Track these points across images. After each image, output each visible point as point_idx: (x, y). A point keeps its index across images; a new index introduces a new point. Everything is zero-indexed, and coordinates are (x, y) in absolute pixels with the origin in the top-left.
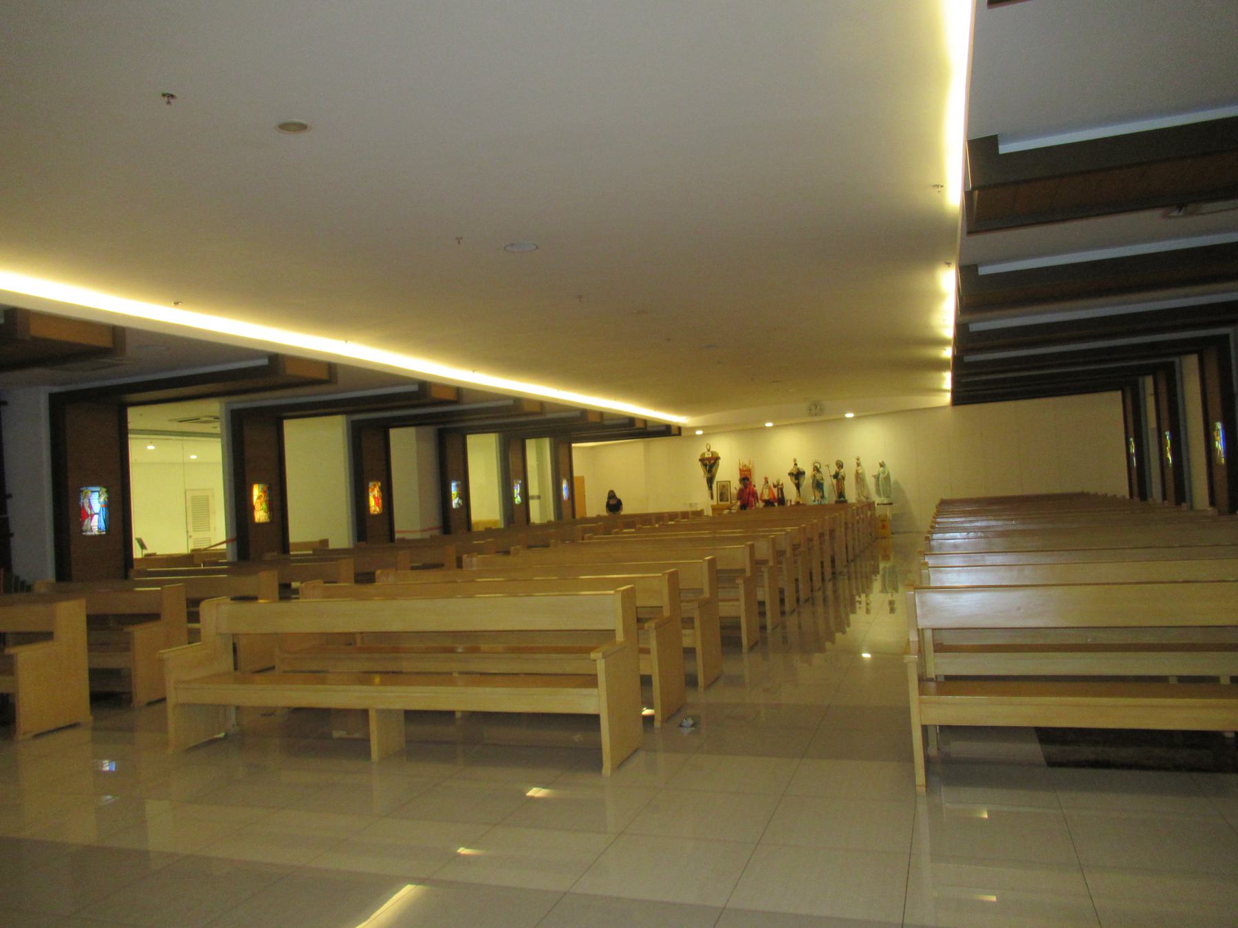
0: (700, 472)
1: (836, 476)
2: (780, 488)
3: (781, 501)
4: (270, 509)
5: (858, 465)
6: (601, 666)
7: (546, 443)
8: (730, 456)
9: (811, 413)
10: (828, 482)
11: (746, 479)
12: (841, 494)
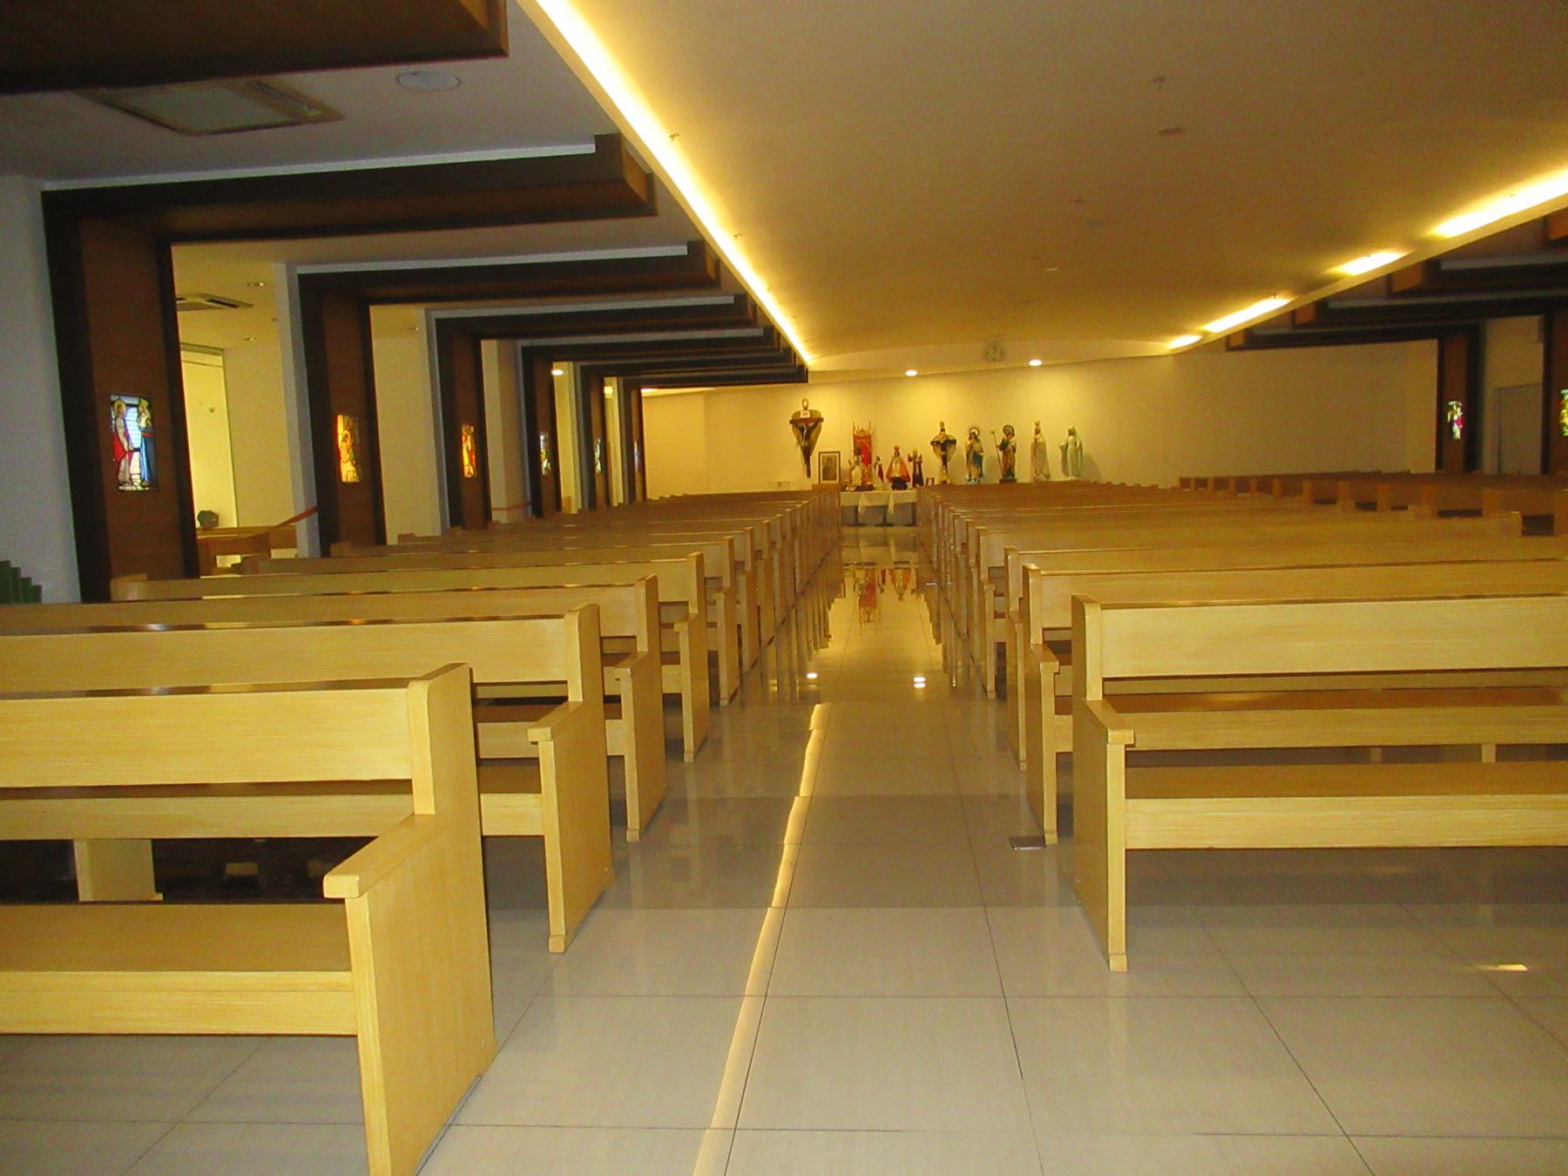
0: (790, 437)
1: (1003, 446)
2: (916, 461)
3: (918, 479)
4: (358, 462)
5: (1038, 432)
6: (547, 754)
7: (1530, 325)
8: (838, 415)
9: (986, 356)
10: (991, 452)
11: (863, 447)
12: (1009, 471)
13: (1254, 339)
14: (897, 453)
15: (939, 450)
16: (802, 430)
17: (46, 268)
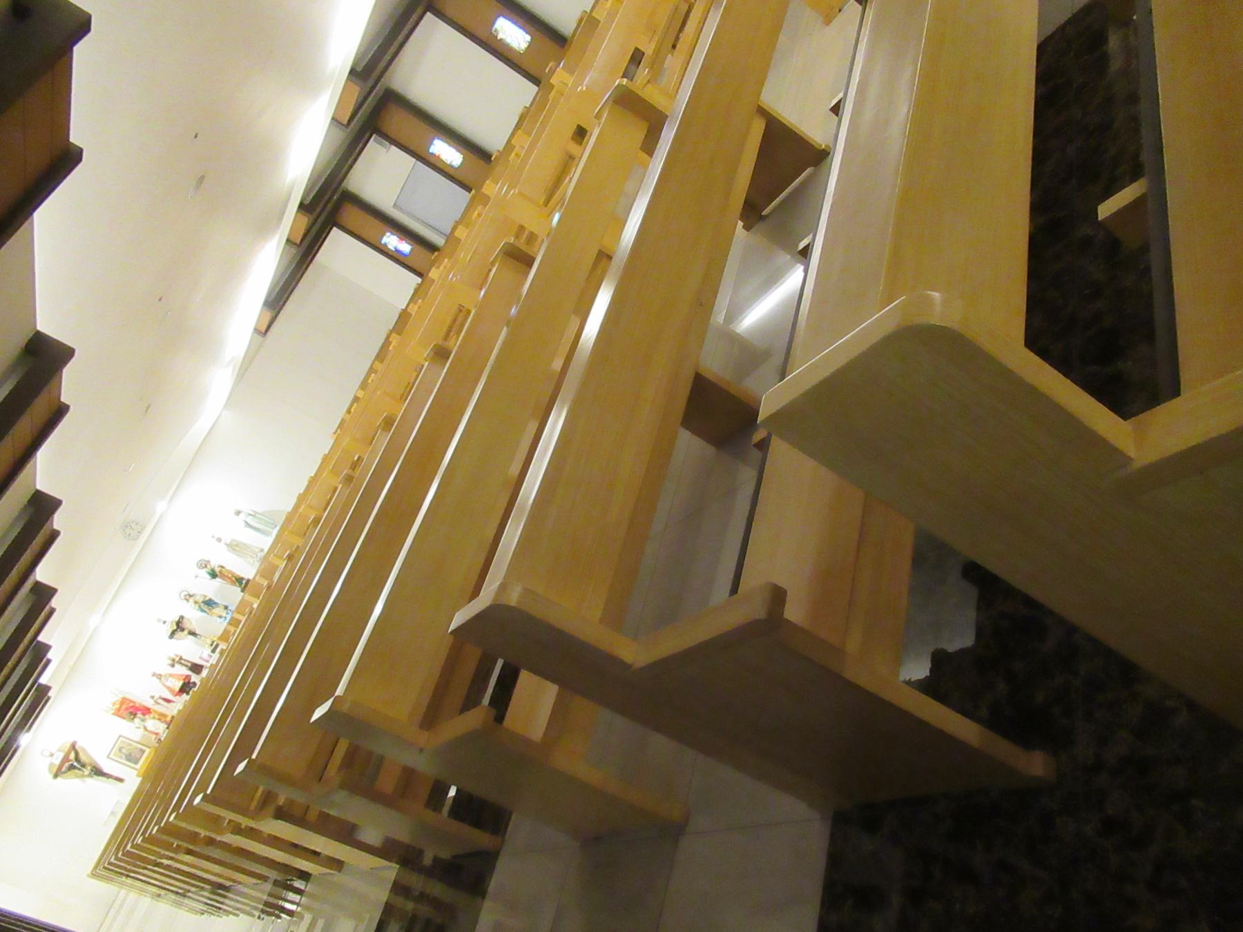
0: (73, 784)
2: (177, 661)
3: (196, 668)
5: (219, 540)
10: (212, 588)
13: (278, 300)
14: (159, 676)
15: (66, 759)
16: (72, 767)
17: (322, 147)
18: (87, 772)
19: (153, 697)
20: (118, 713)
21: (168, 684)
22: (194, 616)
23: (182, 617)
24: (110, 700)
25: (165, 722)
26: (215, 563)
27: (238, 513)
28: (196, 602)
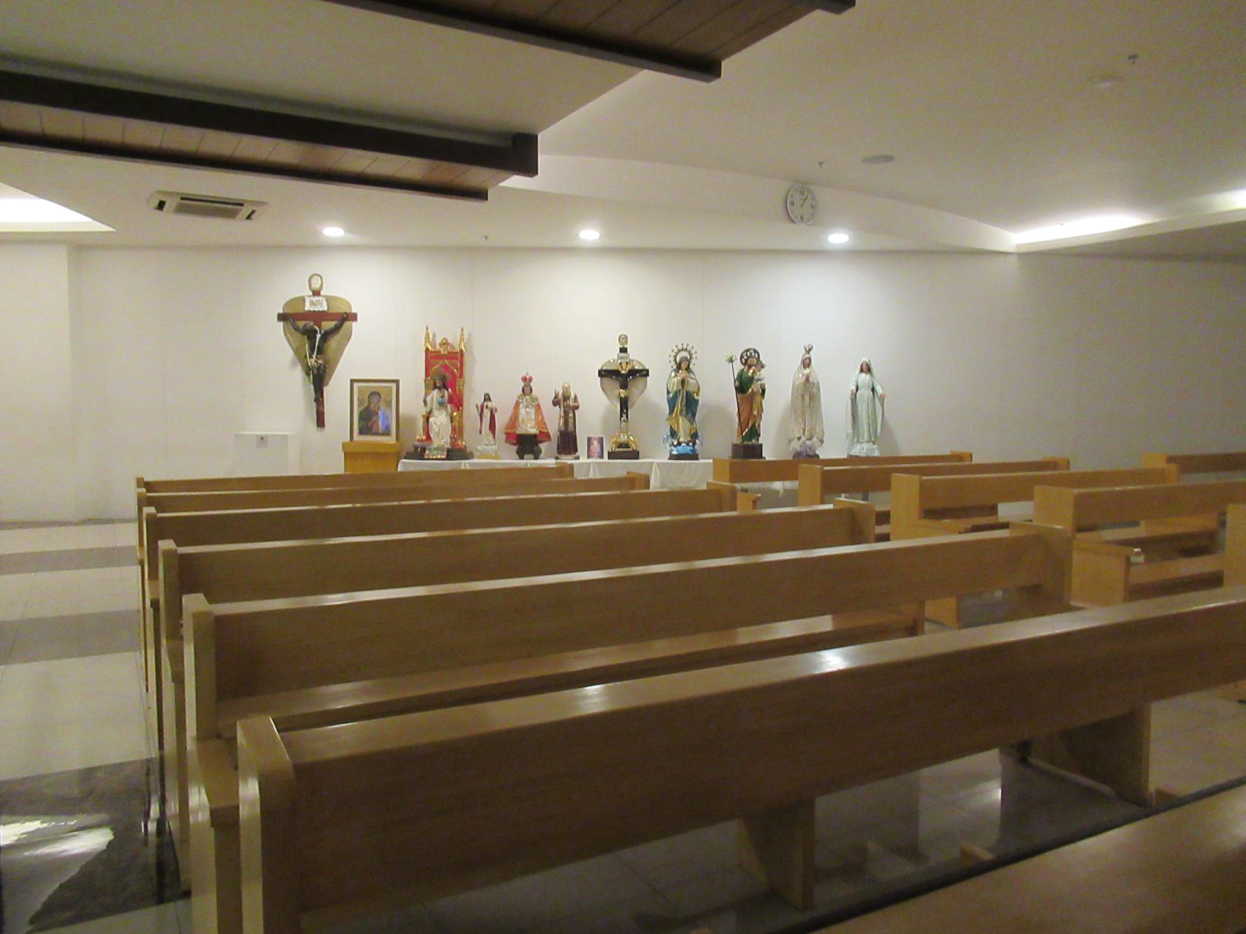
0: (278, 350)
2: (566, 403)
3: (567, 443)
10: (716, 389)
14: (527, 390)
15: (319, 316)
16: (310, 334)
18: (312, 362)
19: (487, 398)
20: (431, 357)
21: (522, 411)
22: (656, 391)
23: (645, 373)
24: (447, 332)
25: (453, 444)
26: (767, 376)
27: (866, 369)
28: (683, 382)
